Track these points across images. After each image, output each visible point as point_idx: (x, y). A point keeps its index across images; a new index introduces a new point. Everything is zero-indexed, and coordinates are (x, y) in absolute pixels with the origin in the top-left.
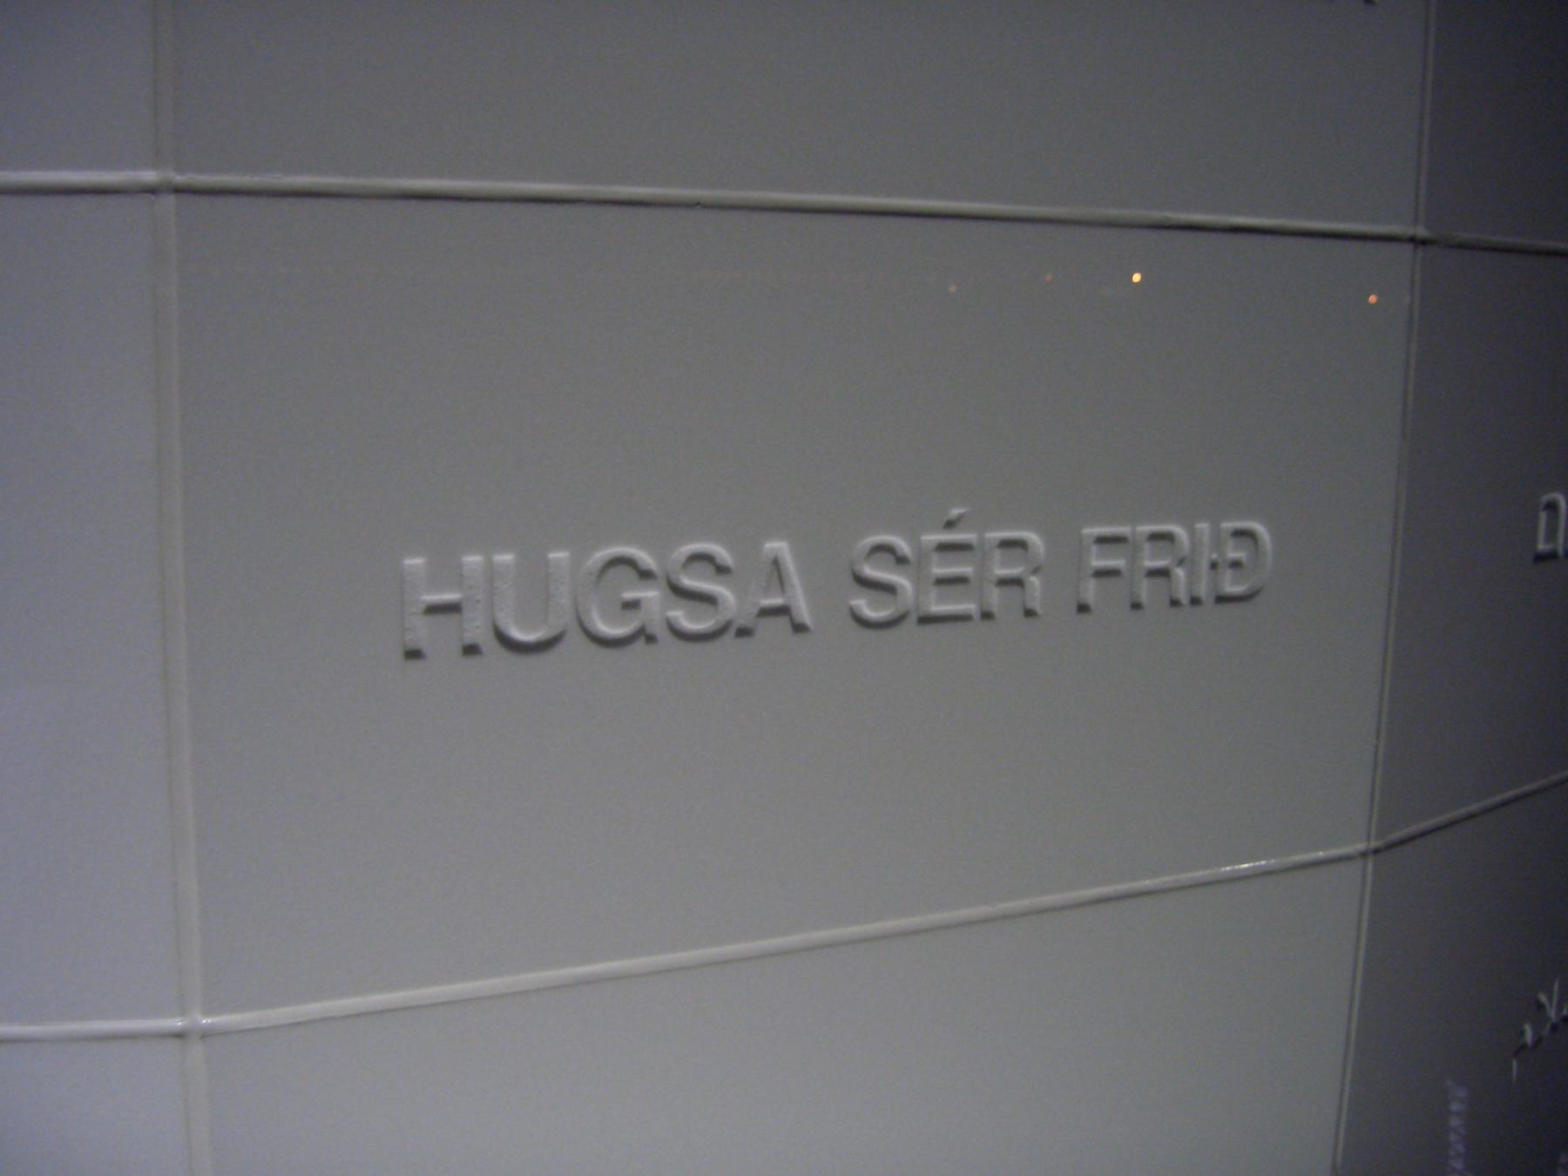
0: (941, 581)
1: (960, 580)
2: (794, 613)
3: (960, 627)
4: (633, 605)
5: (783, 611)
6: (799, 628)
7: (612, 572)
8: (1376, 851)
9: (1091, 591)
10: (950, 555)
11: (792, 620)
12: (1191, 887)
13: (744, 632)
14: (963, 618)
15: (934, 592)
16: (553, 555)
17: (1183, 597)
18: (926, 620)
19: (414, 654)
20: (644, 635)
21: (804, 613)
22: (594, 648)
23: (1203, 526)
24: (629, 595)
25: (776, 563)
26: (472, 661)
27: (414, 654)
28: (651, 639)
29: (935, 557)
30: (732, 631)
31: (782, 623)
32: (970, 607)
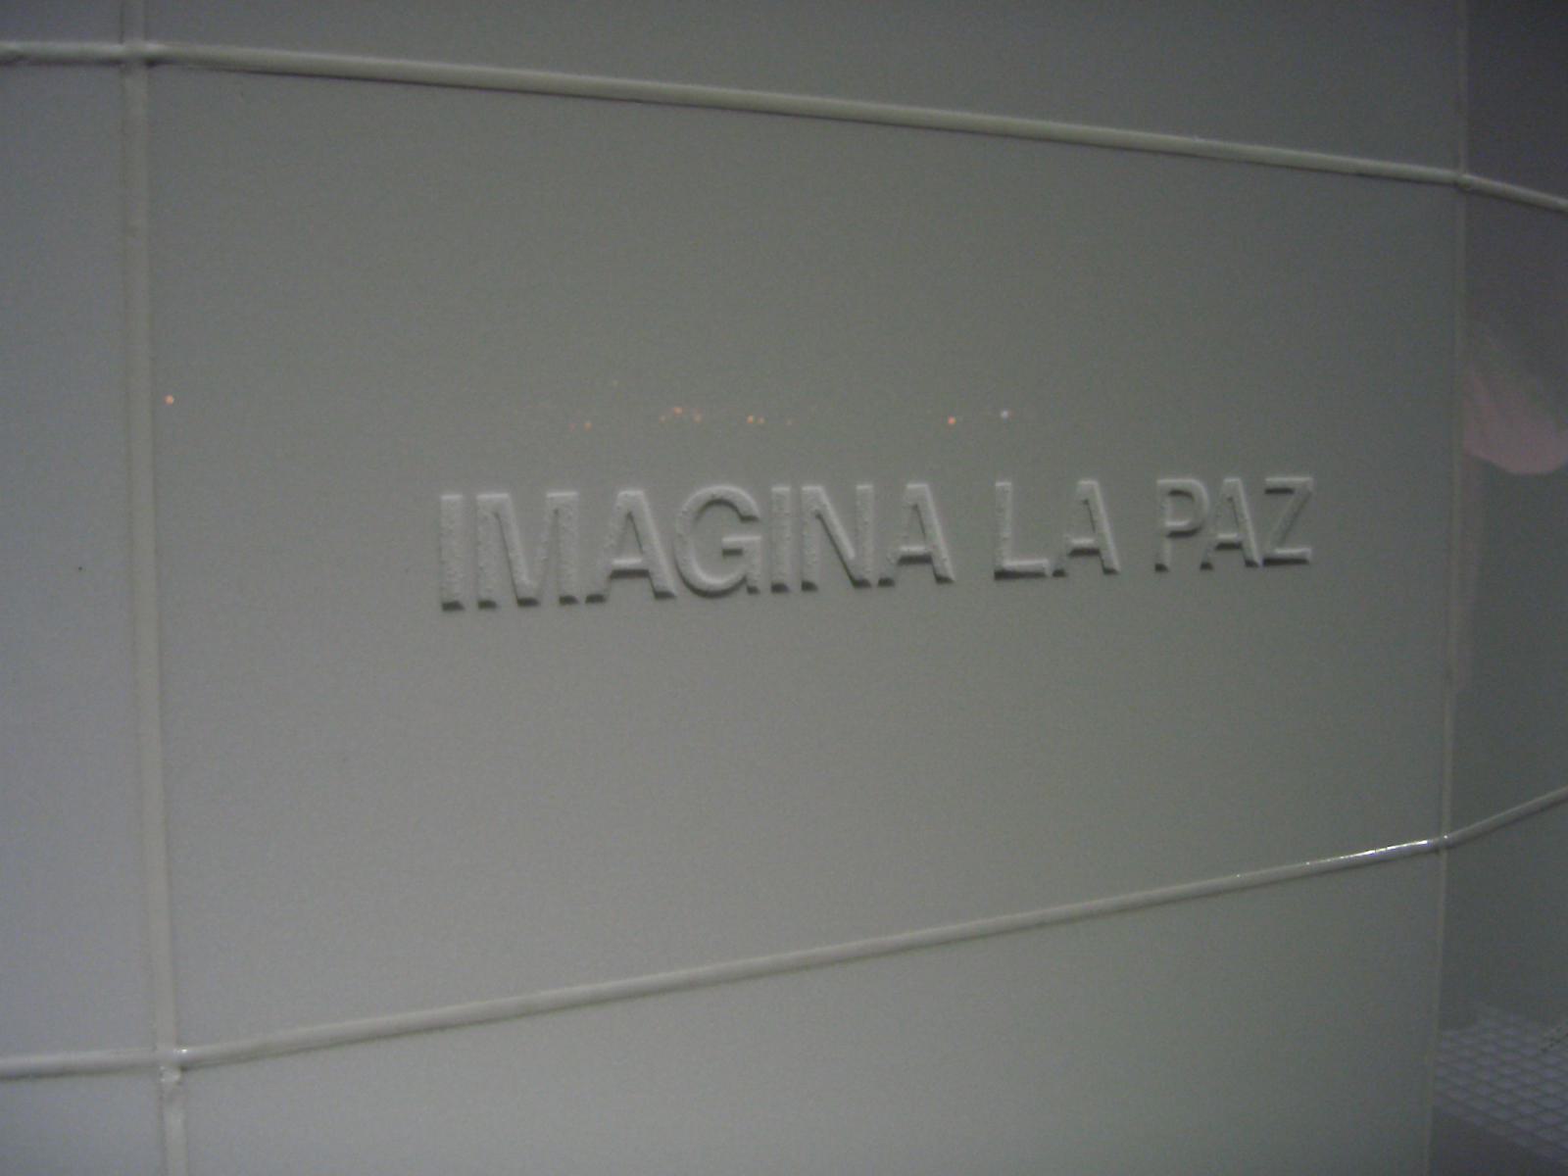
2: (937, 564)
3: (1295, 568)
4: (733, 553)
5: (641, 574)
7: (717, 511)
9: (1168, 550)
13: (595, 599)
14: (1037, 575)
22: (698, 600)
23: (782, 489)
24: (731, 540)
26: (455, 616)
28: (752, 590)
31: (639, 586)
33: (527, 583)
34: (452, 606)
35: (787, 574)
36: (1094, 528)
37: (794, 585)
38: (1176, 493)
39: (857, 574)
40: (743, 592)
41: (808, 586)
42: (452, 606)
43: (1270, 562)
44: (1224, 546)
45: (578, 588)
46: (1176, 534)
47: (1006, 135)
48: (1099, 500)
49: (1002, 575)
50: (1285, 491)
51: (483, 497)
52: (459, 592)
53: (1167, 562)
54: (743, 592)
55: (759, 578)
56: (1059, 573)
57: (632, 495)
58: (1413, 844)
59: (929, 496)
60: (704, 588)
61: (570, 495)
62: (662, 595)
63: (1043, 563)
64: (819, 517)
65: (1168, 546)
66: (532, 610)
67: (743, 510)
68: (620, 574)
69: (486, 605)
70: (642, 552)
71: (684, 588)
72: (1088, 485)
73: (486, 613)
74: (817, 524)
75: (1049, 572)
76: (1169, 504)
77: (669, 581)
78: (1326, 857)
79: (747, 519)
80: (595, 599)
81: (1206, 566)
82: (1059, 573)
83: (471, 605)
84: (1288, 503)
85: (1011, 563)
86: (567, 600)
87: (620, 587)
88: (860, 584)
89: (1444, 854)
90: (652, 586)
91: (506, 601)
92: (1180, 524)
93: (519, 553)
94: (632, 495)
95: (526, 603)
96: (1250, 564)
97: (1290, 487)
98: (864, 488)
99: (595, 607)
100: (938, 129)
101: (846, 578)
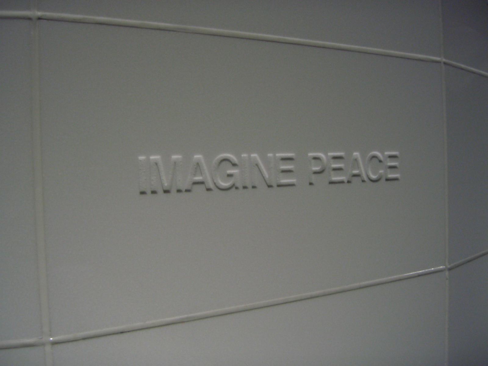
1: (340, 169)
4: (230, 176)
5: (202, 183)
7: (224, 163)
8: (450, 269)
10: (336, 160)
12: (391, 282)
13: (188, 191)
14: (342, 182)
16: (243, 155)
17: (249, 186)
18: (388, 180)
19: (311, 184)
20: (233, 187)
23: (244, 155)
24: (229, 172)
25: (356, 160)
27: (311, 184)
28: (237, 188)
29: (388, 159)
30: (383, 180)
31: (202, 187)
34: (143, 193)
36: (201, 174)
37: (149, 192)
38: (315, 158)
40: (234, 189)
41: (254, 187)
42: (143, 193)
43: (279, 186)
45: (183, 188)
46: (315, 173)
47: (324, 47)
49: (332, 183)
51: (152, 157)
53: (313, 181)
55: (238, 184)
56: (349, 182)
57: (198, 157)
58: (403, 275)
60: (223, 188)
62: (209, 190)
64: (257, 165)
65: (314, 177)
66: (168, 194)
67: (233, 163)
69: (154, 192)
70: (201, 174)
73: (154, 195)
75: (346, 181)
77: (211, 186)
78: (405, 273)
79: (234, 165)
80: (188, 191)
82: (349, 182)
86: (179, 191)
87: (196, 187)
88: (270, 186)
89: (447, 273)
90: (206, 187)
91: (160, 192)
92: (317, 169)
93: (164, 178)
94: (198, 157)
95: (166, 191)
97: (321, 158)
99: (188, 193)
100: (224, 36)
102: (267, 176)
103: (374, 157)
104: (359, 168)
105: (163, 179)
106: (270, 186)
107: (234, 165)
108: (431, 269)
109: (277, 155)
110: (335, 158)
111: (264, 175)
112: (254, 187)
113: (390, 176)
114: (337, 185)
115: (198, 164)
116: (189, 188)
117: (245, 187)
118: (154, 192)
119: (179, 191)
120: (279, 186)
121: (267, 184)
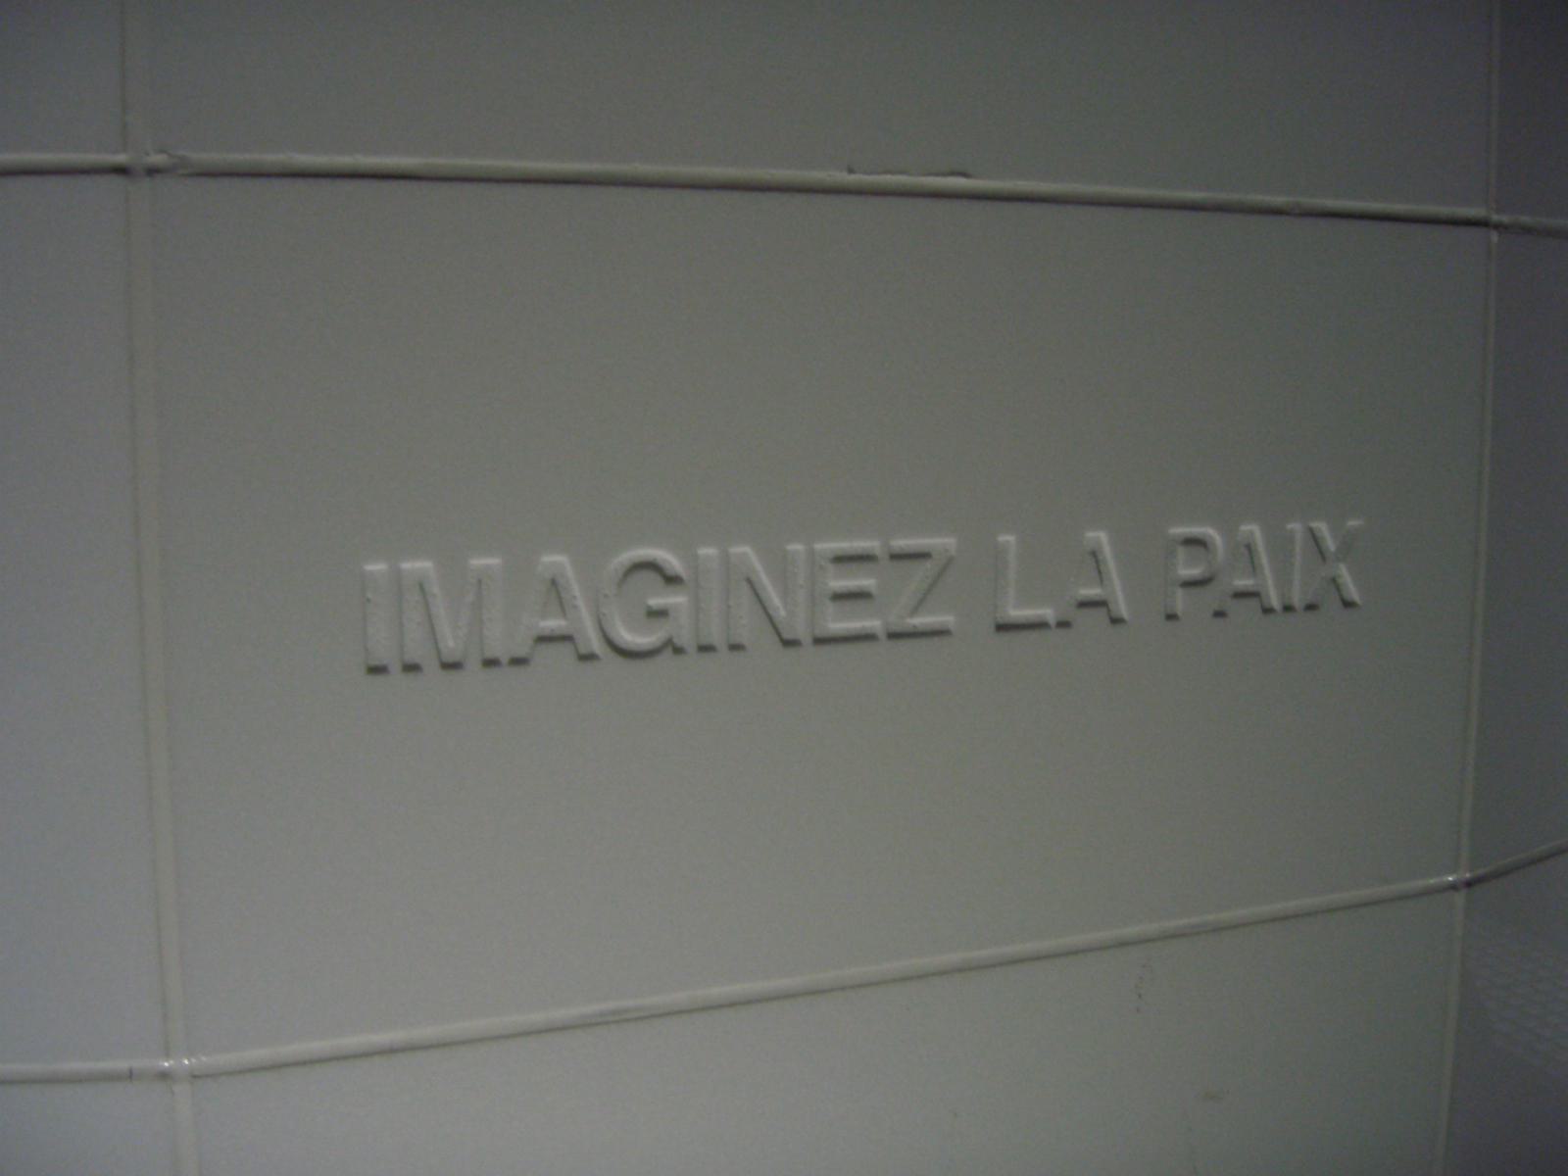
0: (840, 597)
2: (1112, 606)
3: (1033, 636)
4: (660, 614)
5: (567, 638)
6: (1116, 621)
8: (1469, 884)
9: (1180, 601)
11: (1109, 611)
13: (518, 662)
14: (1040, 625)
15: (831, 608)
21: (1123, 609)
22: (619, 660)
23: (707, 551)
24: (655, 602)
25: (1094, 554)
26: (379, 679)
27: (1171, 617)
28: (678, 651)
31: (1100, 614)
32: (873, 624)
33: (451, 644)
34: (377, 670)
35: (715, 635)
36: (1102, 581)
39: (786, 636)
41: (735, 647)
42: (377, 670)
43: (820, 641)
44: (1240, 595)
45: (497, 649)
46: (1189, 584)
48: (1107, 552)
49: (1003, 628)
50: (922, 556)
51: (406, 566)
52: (383, 654)
54: (668, 653)
55: (685, 639)
56: (1063, 624)
57: (556, 560)
59: (570, 572)
60: (624, 646)
61: (494, 561)
62: (588, 657)
63: (1048, 613)
65: (1180, 593)
67: (670, 572)
68: (544, 639)
70: (564, 613)
71: (608, 650)
72: (1100, 537)
74: (745, 588)
75: (881, 634)
76: (1181, 552)
77: (596, 645)
79: (672, 580)
80: (518, 662)
81: (1219, 614)
82: (1063, 624)
83: (395, 668)
84: (923, 571)
85: (1016, 614)
86: (491, 663)
88: (789, 643)
92: (1195, 572)
94: (556, 560)
96: (1268, 611)
98: (1008, 539)
101: (777, 639)
102: (780, 612)
103: (652, 566)
104: (1254, 568)
105: (604, 615)
106: (789, 643)
107: (672, 580)
108: (1444, 879)
109: (818, 546)
110: (841, 559)
111: (771, 612)
112: (735, 647)
113: (838, 626)
114: (923, 643)
115: (554, 582)
116: (521, 651)
117: (706, 649)
118: (411, 668)
119: (491, 663)
120: (820, 641)
121: (778, 634)
